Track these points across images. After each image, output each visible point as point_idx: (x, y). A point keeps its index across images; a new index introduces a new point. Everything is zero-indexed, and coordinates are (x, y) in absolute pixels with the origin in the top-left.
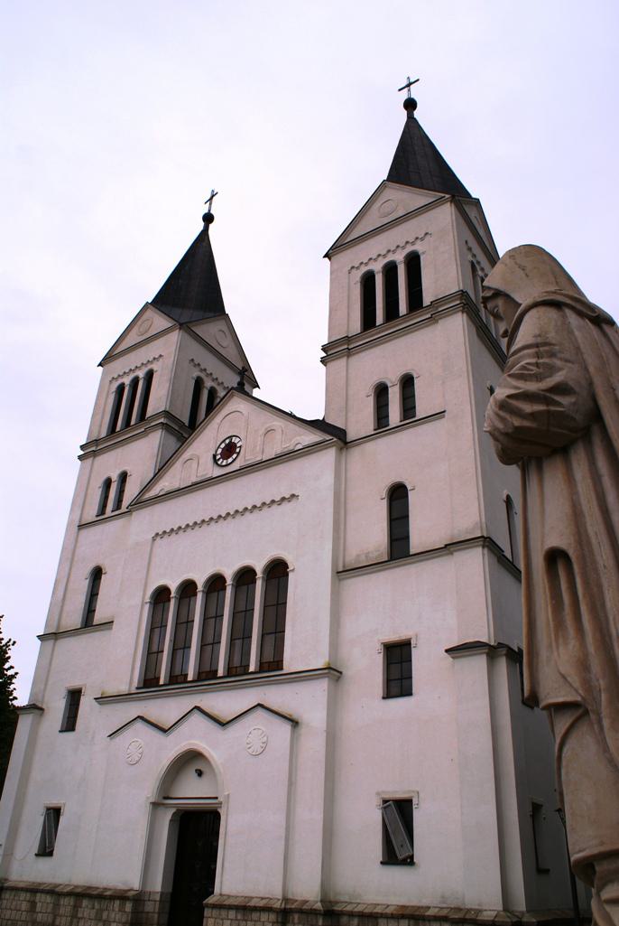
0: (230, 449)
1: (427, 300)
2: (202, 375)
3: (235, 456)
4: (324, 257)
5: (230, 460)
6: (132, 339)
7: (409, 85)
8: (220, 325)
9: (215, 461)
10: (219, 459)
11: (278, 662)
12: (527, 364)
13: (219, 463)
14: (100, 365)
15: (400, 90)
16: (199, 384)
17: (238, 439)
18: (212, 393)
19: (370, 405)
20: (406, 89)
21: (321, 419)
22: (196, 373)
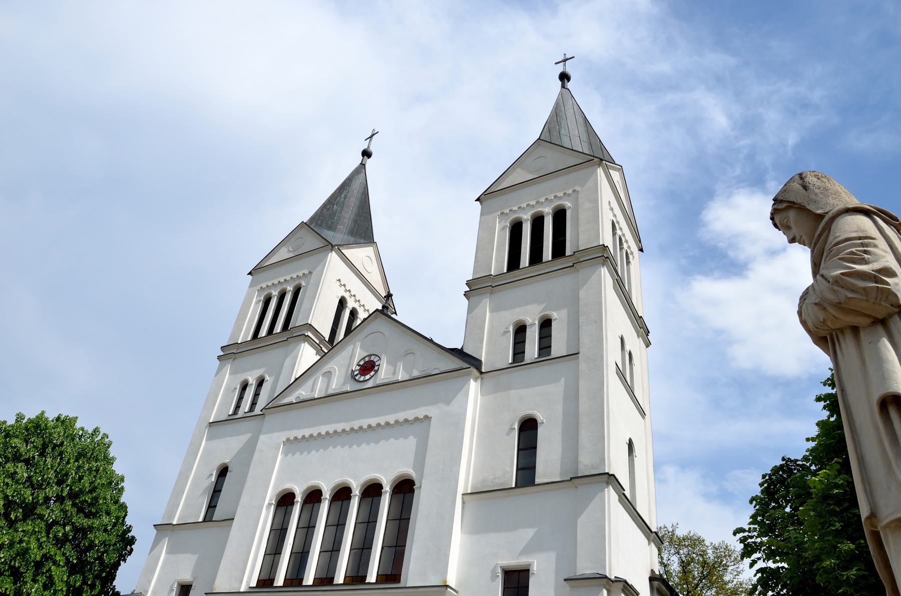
0: (368, 367)
1: (568, 252)
2: (347, 295)
3: (372, 373)
4: (476, 200)
5: (368, 377)
6: (283, 254)
7: (565, 61)
8: (369, 251)
9: (353, 377)
10: (357, 375)
11: (362, 577)
12: (842, 274)
13: (357, 378)
14: (250, 273)
15: (366, 140)
16: (342, 303)
17: (377, 358)
18: (353, 314)
19: (521, 341)
20: (562, 63)
21: (460, 348)
22: (341, 292)
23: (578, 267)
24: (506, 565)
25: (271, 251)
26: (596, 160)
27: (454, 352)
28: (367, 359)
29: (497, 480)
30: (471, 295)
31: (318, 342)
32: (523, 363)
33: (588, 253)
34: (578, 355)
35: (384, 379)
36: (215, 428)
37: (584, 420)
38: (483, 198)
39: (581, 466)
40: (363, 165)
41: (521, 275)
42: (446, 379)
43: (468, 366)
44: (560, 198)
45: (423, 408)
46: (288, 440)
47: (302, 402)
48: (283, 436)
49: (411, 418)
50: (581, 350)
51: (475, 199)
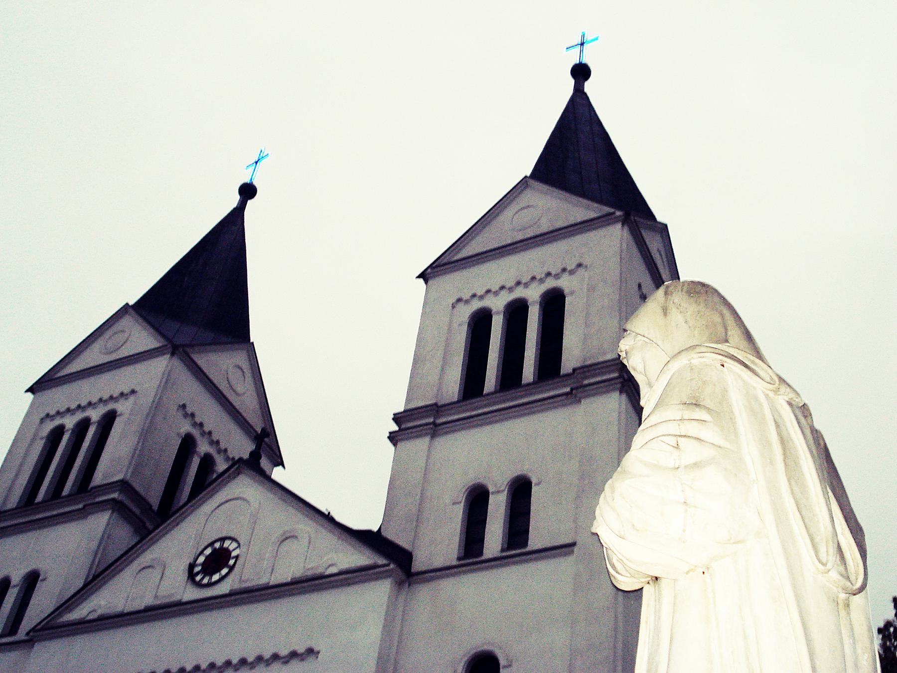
2: (195, 432)
3: (225, 571)
4: (419, 277)
5: (216, 577)
8: (239, 358)
9: (191, 576)
10: (198, 573)
16: (187, 444)
17: (234, 545)
22: (186, 427)
27: (366, 538)
28: (217, 545)
31: (137, 511)
32: (524, 550)
38: (429, 274)
40: (579, 91)
43: (385, 562)
51: (417, 275)
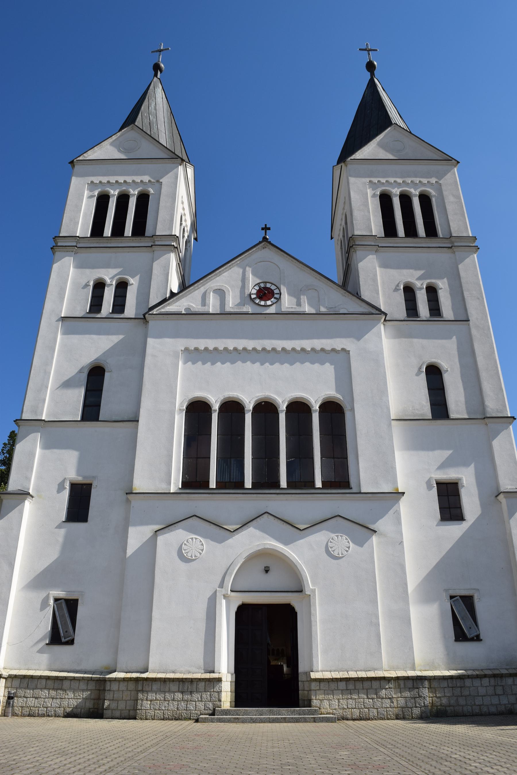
23: (455, 250)
24: (439, 478)
25: (426, 143)
26: (453, 161)
29: (416, 412)
30: (359, 249)
33: (466, 240)
34: (468, 322)
35: (287, 308)
36: (68, 323)
37: (484, 375)
39: (488, 410)
41: (401, 243)
42: (357, 320)
44: (407, 184)
45: (343, 340)
46: (187, 349)
47: (190, 314)
48: (181, 344)
49: (328, 348)
50: (470, 319)
51: (69, 162)
